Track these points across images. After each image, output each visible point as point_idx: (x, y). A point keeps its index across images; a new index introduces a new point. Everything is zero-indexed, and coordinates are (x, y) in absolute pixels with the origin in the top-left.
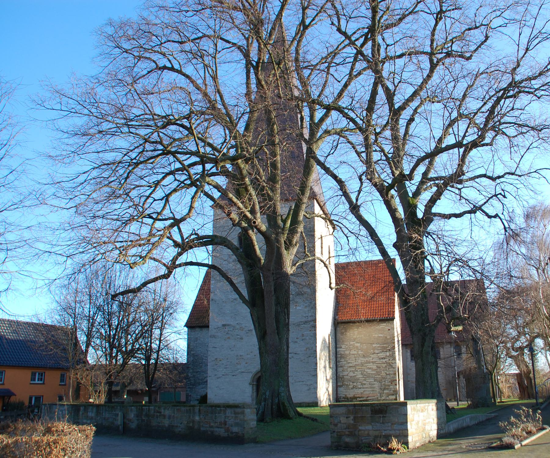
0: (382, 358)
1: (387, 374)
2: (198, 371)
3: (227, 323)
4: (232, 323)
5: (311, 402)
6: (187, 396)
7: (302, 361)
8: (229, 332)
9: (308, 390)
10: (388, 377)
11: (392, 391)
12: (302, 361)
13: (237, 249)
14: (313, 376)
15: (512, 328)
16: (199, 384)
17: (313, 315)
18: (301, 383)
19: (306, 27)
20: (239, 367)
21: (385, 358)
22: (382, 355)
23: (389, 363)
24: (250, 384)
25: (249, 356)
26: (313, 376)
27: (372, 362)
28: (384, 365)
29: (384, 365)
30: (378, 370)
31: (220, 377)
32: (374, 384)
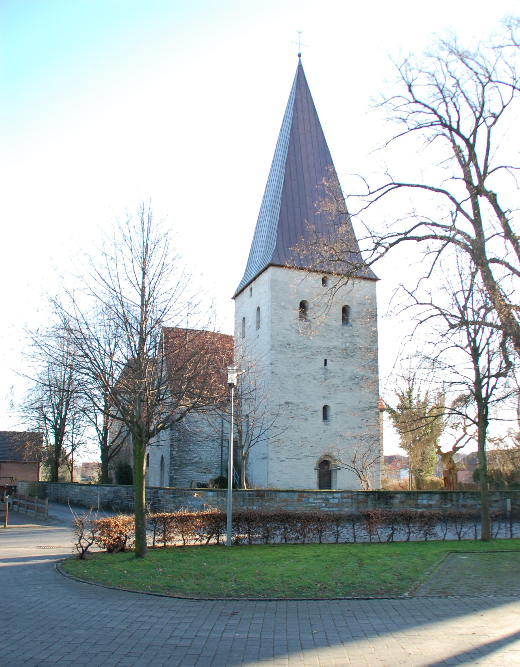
3: (290, 401)
4: (295, 401)
6: (170, 478)
8: (293, 411)
15: (270, 581)
17: (369, 374)
19: (478, 126)
20: (303, 450)
24: (315, 469)
25: (314, 439)
31: (282, 461)
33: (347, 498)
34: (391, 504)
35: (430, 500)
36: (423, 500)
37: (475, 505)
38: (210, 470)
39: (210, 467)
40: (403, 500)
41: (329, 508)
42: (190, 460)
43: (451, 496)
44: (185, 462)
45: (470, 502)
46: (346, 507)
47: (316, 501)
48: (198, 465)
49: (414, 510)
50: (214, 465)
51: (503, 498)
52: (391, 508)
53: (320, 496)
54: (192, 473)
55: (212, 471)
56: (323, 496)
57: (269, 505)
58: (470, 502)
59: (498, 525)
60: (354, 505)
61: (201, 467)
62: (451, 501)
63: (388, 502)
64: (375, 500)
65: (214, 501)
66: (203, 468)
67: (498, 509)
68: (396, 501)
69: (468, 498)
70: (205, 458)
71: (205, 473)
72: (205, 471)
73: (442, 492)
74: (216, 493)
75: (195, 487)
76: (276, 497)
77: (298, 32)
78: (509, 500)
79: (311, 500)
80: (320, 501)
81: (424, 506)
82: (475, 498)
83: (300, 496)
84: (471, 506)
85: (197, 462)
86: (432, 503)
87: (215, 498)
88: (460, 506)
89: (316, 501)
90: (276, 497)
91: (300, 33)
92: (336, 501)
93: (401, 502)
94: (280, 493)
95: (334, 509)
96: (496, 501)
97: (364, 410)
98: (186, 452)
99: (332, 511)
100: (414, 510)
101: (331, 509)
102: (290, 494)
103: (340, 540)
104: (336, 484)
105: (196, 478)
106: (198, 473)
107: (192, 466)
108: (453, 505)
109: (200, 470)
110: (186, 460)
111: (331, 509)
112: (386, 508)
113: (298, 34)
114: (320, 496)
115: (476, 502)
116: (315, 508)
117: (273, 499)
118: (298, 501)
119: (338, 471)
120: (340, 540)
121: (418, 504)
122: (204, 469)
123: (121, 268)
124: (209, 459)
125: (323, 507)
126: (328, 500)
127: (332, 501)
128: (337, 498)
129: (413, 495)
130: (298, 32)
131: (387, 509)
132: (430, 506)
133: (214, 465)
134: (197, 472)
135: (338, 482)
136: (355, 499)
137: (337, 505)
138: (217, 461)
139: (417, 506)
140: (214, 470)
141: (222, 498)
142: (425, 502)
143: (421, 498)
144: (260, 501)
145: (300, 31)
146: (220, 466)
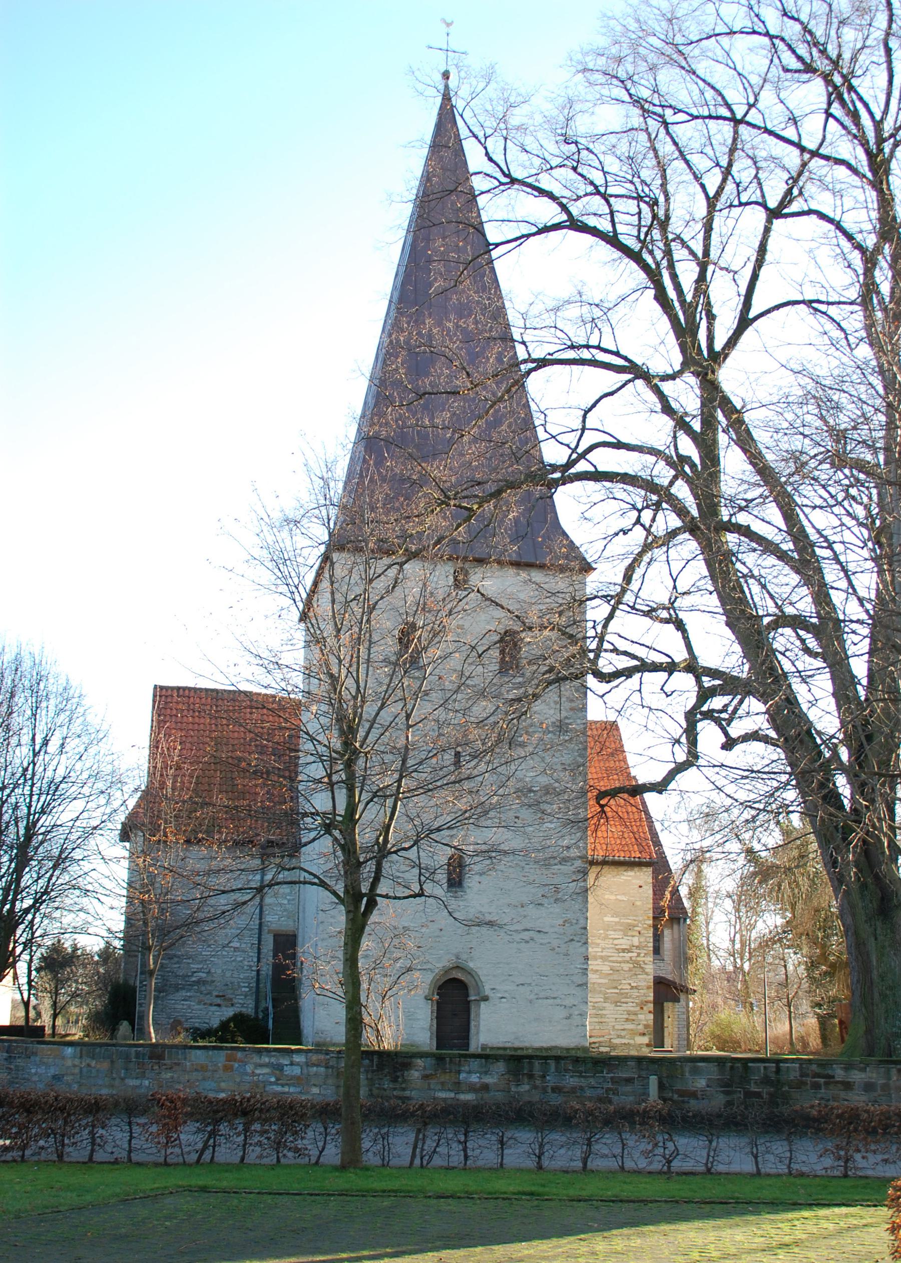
0: (623, 950)
1: (632, 988)
2: (175, 956)
5: (572, 1045)
7: (553, 949)
9: (567, 1018)
10: (635, 993)
11: (641, 1027)
12: (553, 949)
13: (778, 740)
14: (579, 985)
16: (177, 988)
18: (550, 1001)
21: (629, 951)
22: (624, 943)
23: (637, 963)
24: (426, 998)
26: (579, 985)
27: (601, 957)
28: (626, 967)
29: (626, 967)
30: (615, 977)
32: (604, 1009)
33: (318, 1066)
34: (404, 1081)
35: (486, 1073)
36: (469, 1072)
37: (582, 1088)
38: (231, 999)
39: (230, 991)
40: (429, 1072)
41: (283, 1086)
42: (185, 977)
43: (531, 1065)
44: (173, 981)
45: (571, 1081)
46: (315, 1085)
47: (258, 1072)
48: (203, 988)
49: (452, 1095)
50: (240, 987)
51: (644, 1074)
52: (404, 1089)
53: (267, 1060)
54: (189, 1007)
55: (235, 1001)
56: (273, 1060)
57: (172, 1077)
58: (571, 1081)
59: (412, 1137)
60: (330, 1081)
61: (209, 993)
62: (531, 1076)
63: (398, 1077)
64: (373, 1071)
65: (75, 1066)
66: (215, 993)
67: (631, 1098)
68: (415, 1074)
69: (566, 1070)
70: (219, 971)
71: (219, 1005)
72: (218, 1001)
73: (512, 1056)
74: (78, 1049)
75: (125, 1038)
76: (185, 1059)
77: (444, 21)
78: (653, 1080)
79: (249, 1068)
80: (266, 1070)
81: (472, 1088)
82: (581, 1072)
83: (230, 1059)
84: (573, 1090)
85: (199, 982)
86: (489, 1080)
87: (77, 1062)
88: (550, 1091)
89: (258, 1072)
90: (185, 1059)
91: (448, 25)
92: (297, 1071)
93: (426, 1077)
94: (193, 1052)
95: (292, 1090)
96: (629, 1081)
97: (549, 865)
98: (176, 959)
99: (288, 1093)
100: (452, 1095)
101: (286, 1089)
102: (210, 1053)
103: (99, 1156)
104: (478, 1033)
105: (198, 1017)
106: (201, 1007)
107: (189, 990)
108: (535, 1087)
109: (207, 999)
110: (177, 976)
111: (286, 1089)
112: (395, 1089)
113: (444, 26)
114: (267, 1060)
115: (583, 1082)
116: (256, 1083)
117: (178, 1064)
118: (227, 1068)
119: (483, 1004)
120: (99, 1156)
121: (459, 1083)
122: (217, 996)
123: (291, 570)
124: (228, 974)
125: (271, 1083)
126: (280, 1068)
127: (288, 1070)
128: (298, 1064)
129: (451, 1061)
130: (444, 21)
131: (395, 1093)
132: (485, 1087)
133: (240, 987)
134: (199, 1003)
135: (482, 1028)
136: (332, 1067)
137: (297, 1080)
138: (247, 978)
139: (457, 1086)
140: (239, 1000)
141: (88, 1061)
142: (474, 1078)
143: (467, 1068)
144: (156, 1067)
145: (449, 21)
146: (254, 990)
